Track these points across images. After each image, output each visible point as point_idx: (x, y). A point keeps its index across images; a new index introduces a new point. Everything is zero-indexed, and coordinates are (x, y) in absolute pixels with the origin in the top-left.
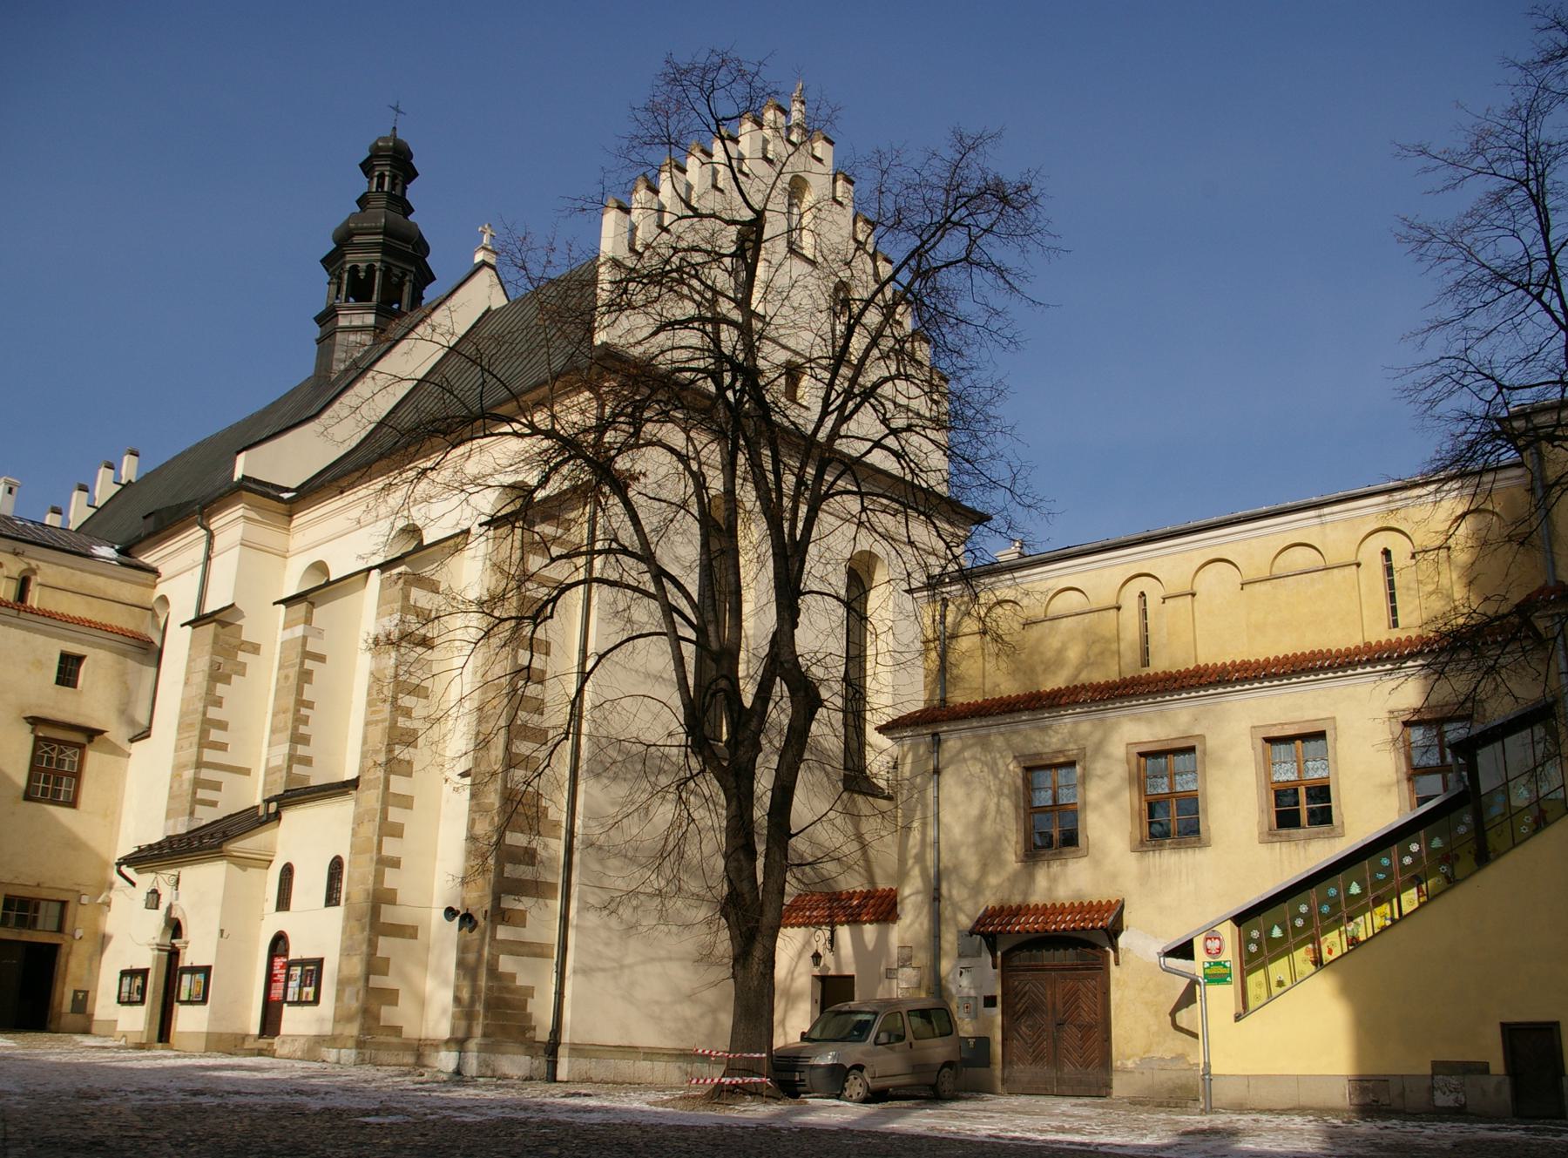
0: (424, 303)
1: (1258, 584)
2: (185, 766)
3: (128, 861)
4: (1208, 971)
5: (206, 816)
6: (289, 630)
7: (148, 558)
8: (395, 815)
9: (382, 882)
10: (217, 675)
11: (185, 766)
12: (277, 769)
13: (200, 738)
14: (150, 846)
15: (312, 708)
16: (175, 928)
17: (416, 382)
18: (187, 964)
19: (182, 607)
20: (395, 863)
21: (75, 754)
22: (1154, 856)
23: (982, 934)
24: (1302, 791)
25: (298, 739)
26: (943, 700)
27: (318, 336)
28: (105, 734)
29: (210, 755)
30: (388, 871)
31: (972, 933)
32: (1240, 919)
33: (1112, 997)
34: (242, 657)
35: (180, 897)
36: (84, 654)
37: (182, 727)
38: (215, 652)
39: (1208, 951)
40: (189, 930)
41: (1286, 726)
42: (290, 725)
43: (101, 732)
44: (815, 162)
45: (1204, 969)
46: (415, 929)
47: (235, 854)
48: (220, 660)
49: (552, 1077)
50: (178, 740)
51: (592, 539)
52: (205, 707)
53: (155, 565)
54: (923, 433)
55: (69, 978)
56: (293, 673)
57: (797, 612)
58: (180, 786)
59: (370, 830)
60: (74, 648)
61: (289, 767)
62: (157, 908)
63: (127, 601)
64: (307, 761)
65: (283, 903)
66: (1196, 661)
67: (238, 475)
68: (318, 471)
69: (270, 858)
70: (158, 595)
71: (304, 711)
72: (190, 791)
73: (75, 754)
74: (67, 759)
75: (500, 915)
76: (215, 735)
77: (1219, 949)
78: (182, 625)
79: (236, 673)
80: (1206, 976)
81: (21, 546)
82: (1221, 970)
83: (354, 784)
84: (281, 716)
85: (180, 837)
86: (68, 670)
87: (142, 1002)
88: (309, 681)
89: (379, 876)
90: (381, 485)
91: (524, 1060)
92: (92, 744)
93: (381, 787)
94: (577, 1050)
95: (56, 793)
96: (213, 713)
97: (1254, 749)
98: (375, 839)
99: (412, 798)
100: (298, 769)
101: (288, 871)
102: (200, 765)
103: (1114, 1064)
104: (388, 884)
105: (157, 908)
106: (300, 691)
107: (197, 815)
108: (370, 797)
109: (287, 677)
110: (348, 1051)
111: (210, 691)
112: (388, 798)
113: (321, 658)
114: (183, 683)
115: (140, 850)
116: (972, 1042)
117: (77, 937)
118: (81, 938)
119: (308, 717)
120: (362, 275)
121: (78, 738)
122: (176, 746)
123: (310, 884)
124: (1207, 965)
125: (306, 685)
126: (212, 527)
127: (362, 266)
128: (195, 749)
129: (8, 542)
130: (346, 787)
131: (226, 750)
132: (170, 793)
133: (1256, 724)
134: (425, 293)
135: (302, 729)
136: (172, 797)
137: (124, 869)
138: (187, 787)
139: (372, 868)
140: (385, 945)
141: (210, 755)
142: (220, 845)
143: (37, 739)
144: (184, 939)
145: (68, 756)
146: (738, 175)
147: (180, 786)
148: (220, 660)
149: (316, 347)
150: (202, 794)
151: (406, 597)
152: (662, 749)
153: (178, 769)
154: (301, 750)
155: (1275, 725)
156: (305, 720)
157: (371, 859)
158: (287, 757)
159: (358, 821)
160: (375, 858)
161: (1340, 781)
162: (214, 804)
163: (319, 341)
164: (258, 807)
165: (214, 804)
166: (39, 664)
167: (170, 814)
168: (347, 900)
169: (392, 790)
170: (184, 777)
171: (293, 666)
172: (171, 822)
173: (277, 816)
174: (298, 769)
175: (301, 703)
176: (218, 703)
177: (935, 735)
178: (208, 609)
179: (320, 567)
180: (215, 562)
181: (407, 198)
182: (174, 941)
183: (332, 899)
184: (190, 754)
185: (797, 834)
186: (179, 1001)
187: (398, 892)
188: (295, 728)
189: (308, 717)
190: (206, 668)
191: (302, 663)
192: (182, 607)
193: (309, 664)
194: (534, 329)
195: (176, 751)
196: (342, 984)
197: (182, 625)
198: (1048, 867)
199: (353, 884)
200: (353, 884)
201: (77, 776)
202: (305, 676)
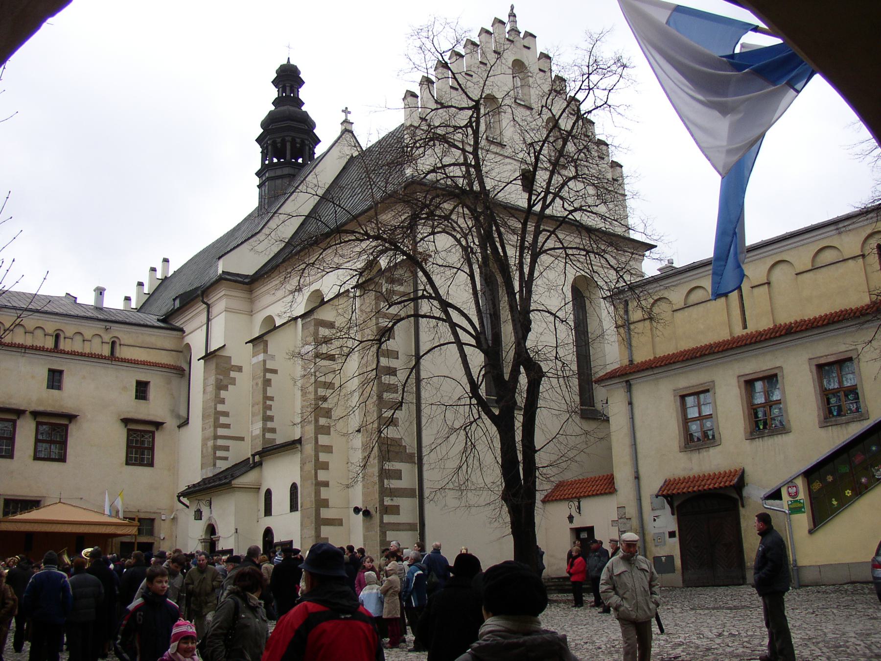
1: (805, 274)
2: (208, 439)
3: (184, 494)
4: (791, 506)
5: (222, 466)
6: (255, 358)
7: (178, 324)
8: (323, 457)
9: (320, 495)
10: (221, 386)
11: (208, 439)
12: (257, 436)
14: (194, 485)
15: (273, 401)
16: (211, 529)
17: (304, 217)
18: (220, 549)
19: (198, 351)
20: (326, 484)
21: (150, 437)
22: (759, 441)
23: (664, 496)
25: (267, 418)
26: (631, 361)
27: (258, 184)
28: (165, 425)
29: (221, 432)
31: (657, 496)
32: (809, 474)
33: (742, 526)
34: (233, 374)
35: (213, 512)
36: (149, 380)
37: (204, 417)
38: (217, 374)
39: (789, 494)
40: (221, 531)
41: (829, 357)
43: (162, 423)
44: (526, 49)
45: (788, 505)
47: (235, 486)
48: (221, 377)
50: (203, 424)
51: (416, 290)
52: (215, 405)
53: (181, 326)
54: (589, 209)
56: (260, 382)
57: (530, 322)
59: (310, 466)
60: (143, 378)
61: (264, 435)
62: (201, 519)
63: (168, 348)
64: (273, 431)
65: (268, 512)
66: (774, 322)
67: (220, 272)
68: (264, 263)
69: (258, 487)
70: (185, 343)
71: (268, 403)
72: (212, 453)
73: (150, 437)
74: (146, 440)
75: (386, 510)
76: (223, 420)
77: (796, 492)
79: (231, 384)
80: (790, 509)
81: (109, 325)
82: (799, 505)
83: (299, 441)
84: (257, 407)
86: (142, 390)
88: (270, 385)
89: (317, 493)
90: (34, 515)
92: (159, 430)
93: (314, 442)
95: (142, 460)
96: (220, 408)
97: (811, 372)
99: (332, 447)
100: (268, 436)
101: (268, 493)
102: (216, 437)
103: (746, 564)
105: (201, 519)
106: (265, 391)
108: (309, 448)
109: (257, 384)
111: (217, 395)
112: (318, 448)
113: (275, 372)
114: (202, 393)
115: (189, 487)
116: (663, 559)
117: (162, 538)
118: (164, 538)
119: (271, 405)
120: (279, 145)
122: (202, 428)
123: (281, 500)
124: (790, 503)
125: (268, 388)
127: (279, 140)
128: (212, 429)
129: (101, 323)
130: (294, 444)
131: (229, 428)
132: (202, 454)
133: (811, 357)
135: (269, 413)
136: (203, 456)
137: (181, 498)
138: (210, 450)
141: (221, 432)
142: (229, 483)
143: (129, 430)
145: (146, 438)
146: (458, 87)
148: (221, 377)
150: (219, 454)
152: (455, 407)
153: (204, 444)
154: (270, 425)
155: (822, 357)
156: (270, 408)
157: (312, 484)
159: (303, 464)
160: (314, 482)
161: (864, 387)
162: (226, 459)
163: (259, 186)
164: (249, 458)
165: (226, 459)
166: (125, 388)
167: (203, 466)
168: (301, 507)
170: (208, 445)
172: (204, 471)
173: (260, 464)
174: (268, 436)
175: (266, 398)
176: (222, 401)
177: (627, 381)
179: (270, 319)
181: (300, 97)
182: (212, 537)
183: (294, 507)
184: (210, 432)
185: (539, 450)
187: (330, 500)
188: (265, 413)
189: (271, 405)
190: (214, 383)
191: (264, 376)
192: (198, 351)
193: (268, 376)
194: (363, 177)
195: (203, 431)
198: (699, 453)
199: (305, 497)
200: (305, 497)
201: (152, 449)
202: (267, 383)
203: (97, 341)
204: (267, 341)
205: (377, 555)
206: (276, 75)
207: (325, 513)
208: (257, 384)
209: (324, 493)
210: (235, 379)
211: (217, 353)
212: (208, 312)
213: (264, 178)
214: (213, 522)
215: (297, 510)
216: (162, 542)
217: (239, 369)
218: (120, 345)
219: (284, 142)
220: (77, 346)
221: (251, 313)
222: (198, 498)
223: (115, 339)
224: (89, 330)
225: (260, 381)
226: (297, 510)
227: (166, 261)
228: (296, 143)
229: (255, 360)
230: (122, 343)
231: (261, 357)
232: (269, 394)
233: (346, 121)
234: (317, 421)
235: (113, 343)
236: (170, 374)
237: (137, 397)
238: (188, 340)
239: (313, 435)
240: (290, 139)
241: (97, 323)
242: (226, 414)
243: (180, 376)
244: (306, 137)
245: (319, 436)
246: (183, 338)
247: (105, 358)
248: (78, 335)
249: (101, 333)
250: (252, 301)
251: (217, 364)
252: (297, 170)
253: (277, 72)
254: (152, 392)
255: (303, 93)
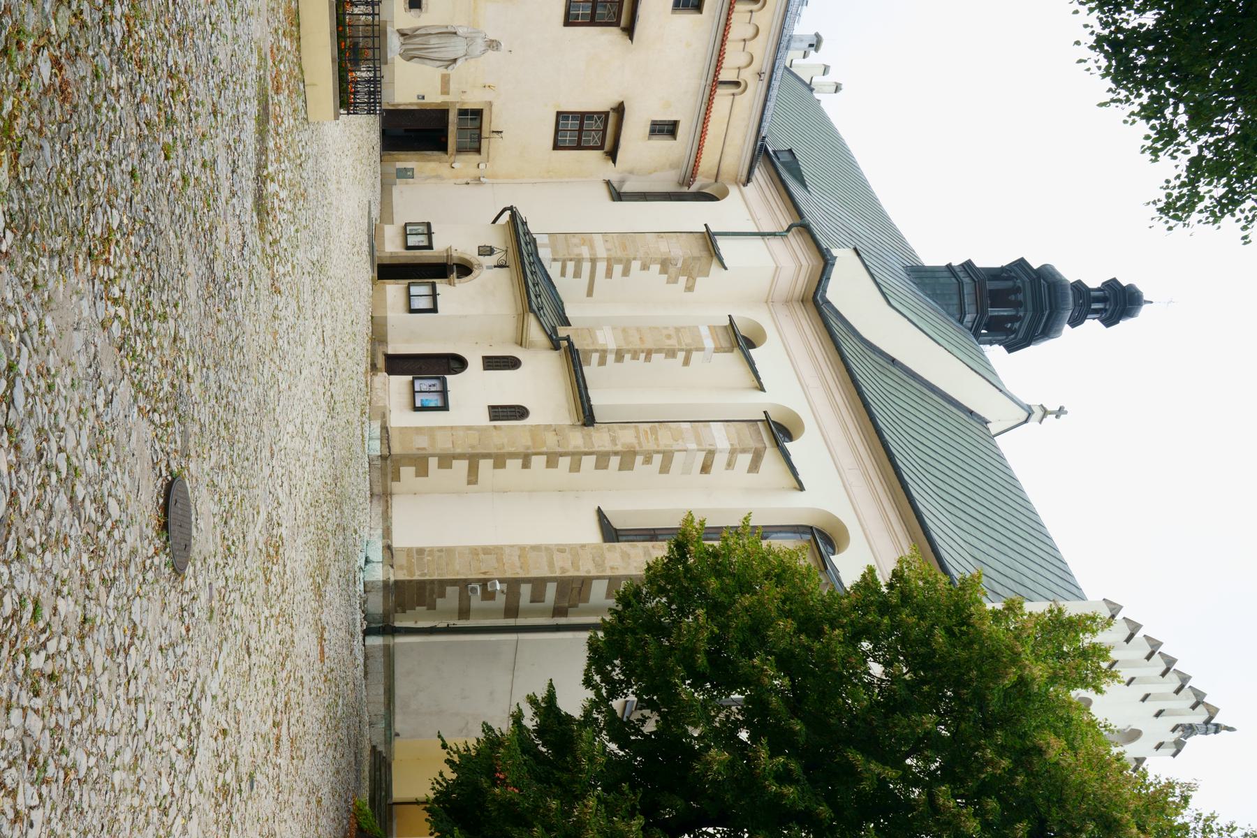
0: (995, 353)
7: (760, 174)
8: (565, 462)
13: (615, 258)
16: (465, 269)
20: (526, 465)
24: (453, 117)
29: (601, 267)
30: (519, 462)
34: (683, 280)
42: (630, 347)
43: (614, 162)
46: (476, 482)
49: (367, 633)
53: (753, 179)
55: (421, 164)
58: (575, 245)
59: (551, 442)
60: (681, 131)
61: (596, 351)
64: (602, 362)
65: (492, 363)
71: (642, 356)
76: (618, 269)
78: (706, 225)
81: (766, 77)
85: (535, 253)
86: (666, 129)
87: (408, 248)
89: (513, 455)
91: (380, 610)
93: (586, 450)
94: (389, 653)
96: (636, 265)
98: (544, 449)
104: (508, 462)
107: (555, 264)
109: (669, 337)
110: (378, 448)
112: (576, 456)
113: (686, 362)
120: (1013, 297)
121: (608, 144)
125: (663, 355)
126: (790, 234)
127: (1020, 297)
134: (996, 346)
135: (628, 357)
137: (508, 213)
138: (576, 251)
139: (521, 450)
140: (461, 466)
141: (601, 267)
143: (607, 114)
144: (457, 281)
147: (575, 245)
148: (679, 265)
149: (944, 264)
150: (571, 266)
151: (744, 451)
153: (586, 237)
154: (611, 358)
157: (528, 449)
158: (604, 348)
159: (556, 430)
162: (563, 274)
165: (563, 274)
168: (495, 427)
169: (584, 458)
171: (679, 343)
173: (556, 346)
174: (595, 357)
175: (649, 354)
176: (645, 267)
178: (721, 243)
180: (758, 242)
186: (414, 379)
188: (628, 351)
193: (681, 355)
196: (430, 431)
197: (706, 225)
202: (671, 353)
203: (743, 59)
204: (732, 351)
205: (426, 574)
206: (1124, 284)
207: (485, 465)
208: (669, 337)
209: (514, 465)
210: (675, 281)
211: (715, 261)
212: (774, 234)
213: (961, 275)
214: (476, 272)
215: (491, 420)
216: (448, 165)
217: (689, 288)
218: (733, 95)
219: (1017, 305)
220: (739, 28)
221: (769, 301)
222: (510, 251)
223: (743, 85)
224: (761, 49)
225: (673, 343)
226: (491, 420)
227: (838, 88)
228: (1013, 323)
229: (704, 331)
230: (736, 97)
231: (709, 344)
232: (654, 356)
233: (1046, 413)
234: (616, 453)
235: (737, 84)
236: (684, 169)
237: (654, 123)
238: (734, 191)
239: (596, 449)
240: (1021, 314)
241: (771, 58)
242: (626, 272)
243: (681, 179)
244: (1021, 335)
245: (594, 457)
246: (737, 183)
247: (716, 75)
248: (754, 31)
249: (756, 66)
250: (788, 302)
251: (699, 259)
252: (970, 325)
253: (1131, 287)
254: (663, 143)
255: (1092, 325)
